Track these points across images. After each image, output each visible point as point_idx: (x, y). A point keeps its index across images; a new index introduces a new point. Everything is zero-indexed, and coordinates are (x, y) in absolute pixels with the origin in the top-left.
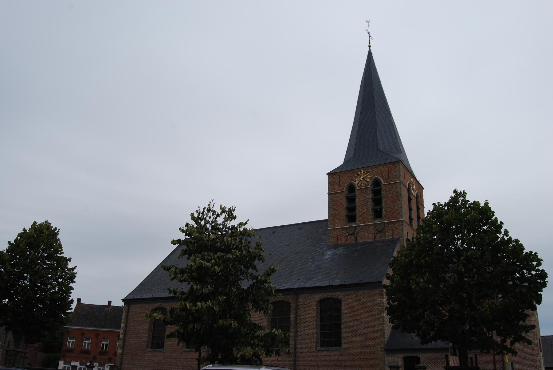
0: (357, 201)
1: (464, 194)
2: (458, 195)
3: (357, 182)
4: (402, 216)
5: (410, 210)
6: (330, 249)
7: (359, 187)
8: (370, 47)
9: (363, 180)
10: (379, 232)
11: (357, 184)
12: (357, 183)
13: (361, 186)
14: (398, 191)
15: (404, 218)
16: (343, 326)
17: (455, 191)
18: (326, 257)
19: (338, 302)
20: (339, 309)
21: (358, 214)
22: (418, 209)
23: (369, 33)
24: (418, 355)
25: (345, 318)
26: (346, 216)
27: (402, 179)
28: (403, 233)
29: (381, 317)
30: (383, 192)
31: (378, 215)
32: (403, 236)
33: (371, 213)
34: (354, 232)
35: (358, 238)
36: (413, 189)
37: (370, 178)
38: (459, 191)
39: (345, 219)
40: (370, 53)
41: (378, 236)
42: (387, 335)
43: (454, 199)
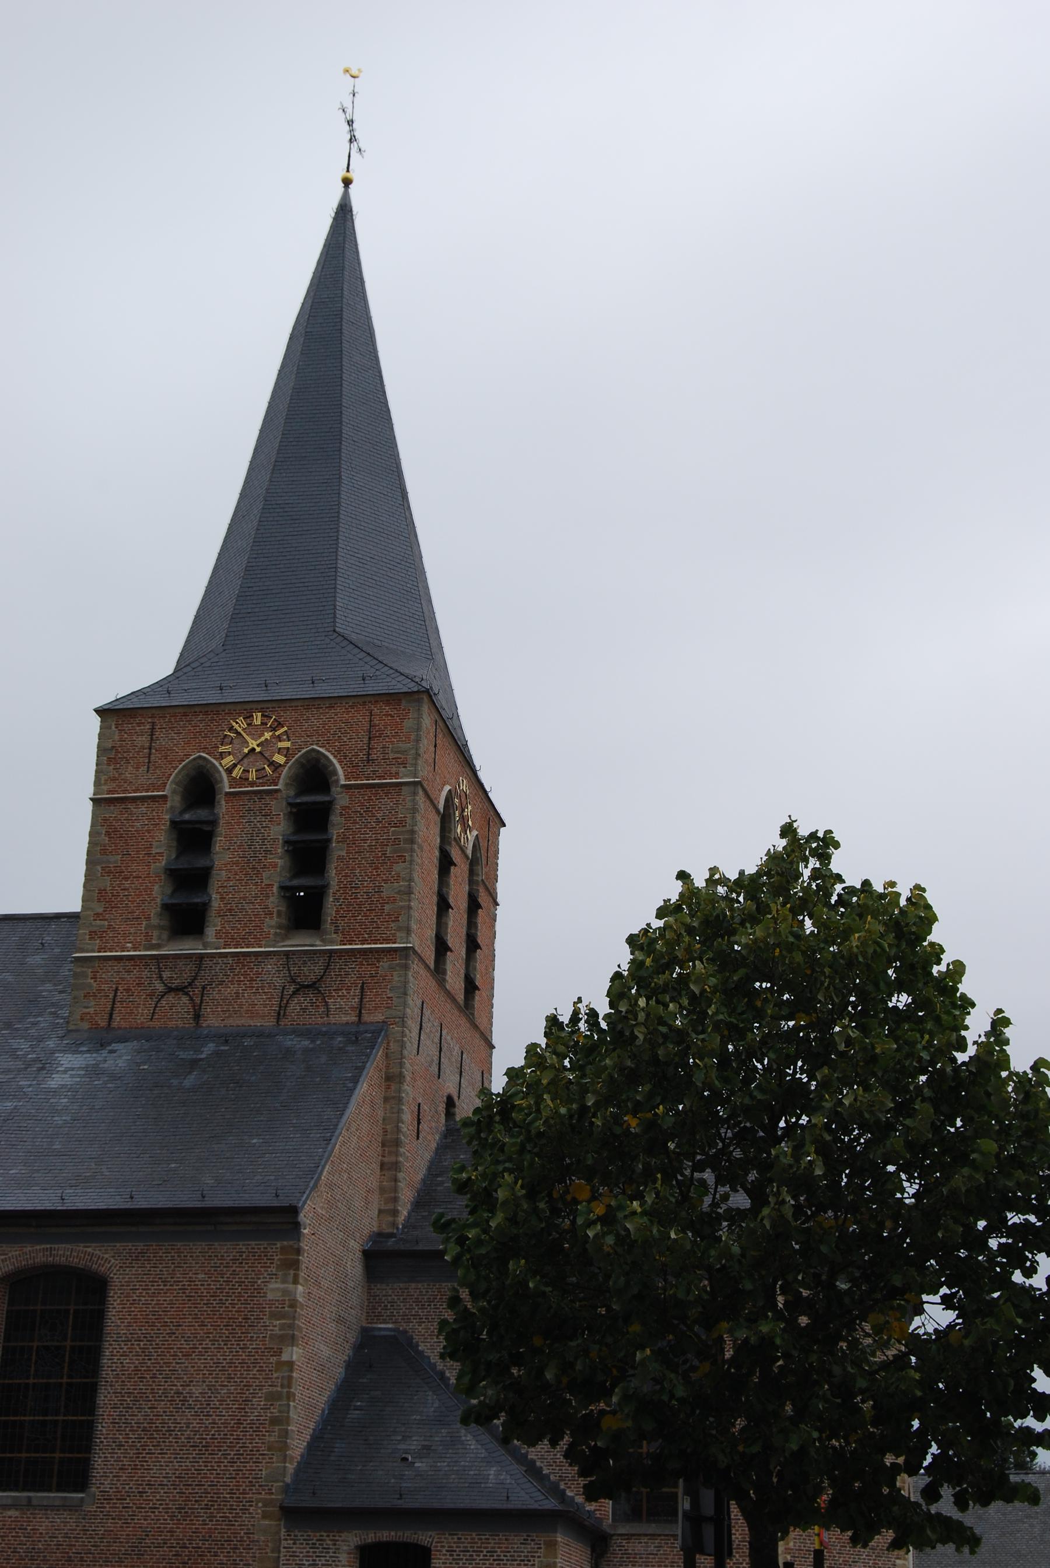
0: (219, 843)
1: (824, 845)
2: (803, 849)
3: (228, 761)
4: (408, 931)
5: (443, 905)
6: (74, 1048)
7: (234, 782)
8: (347, 182)
9: (252, 755)
10: (302, 988)
11: (229, 771)
12: (224, 764)
13: (243, 780)
14: (402, 823)
15: (414, 942)
16: (105, 1398)
17: (788, 830)
18: (56, 1081)
19: (93, 1287)
20: (93, 1323)
21: (216, 904)
22: (474, 906)
23: (350, 123)
24: (424, 1537)
25: (117, 1358)
26: (166, 907)
27: (424, 772)
28: (405, 1005)
29: (280, 1364)
30: (335, 818)
31: (305, 912)
32: (403, 1019)
33: (274, 901)
34: (190, 984)
35: (206, 1010)
36: (463, 820)
37: (287, 753)
38: (803, 831)
39: (155, 921)
40: (344, 213)
41: (294, 1006)
42: (298, 1446)
43: (780, 868)
